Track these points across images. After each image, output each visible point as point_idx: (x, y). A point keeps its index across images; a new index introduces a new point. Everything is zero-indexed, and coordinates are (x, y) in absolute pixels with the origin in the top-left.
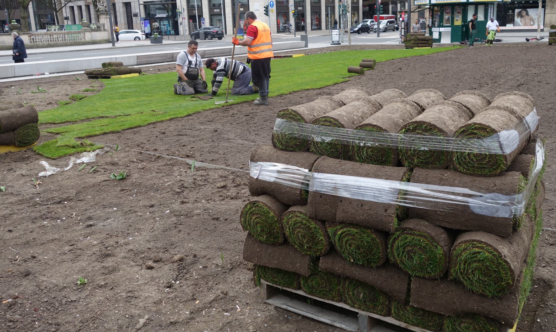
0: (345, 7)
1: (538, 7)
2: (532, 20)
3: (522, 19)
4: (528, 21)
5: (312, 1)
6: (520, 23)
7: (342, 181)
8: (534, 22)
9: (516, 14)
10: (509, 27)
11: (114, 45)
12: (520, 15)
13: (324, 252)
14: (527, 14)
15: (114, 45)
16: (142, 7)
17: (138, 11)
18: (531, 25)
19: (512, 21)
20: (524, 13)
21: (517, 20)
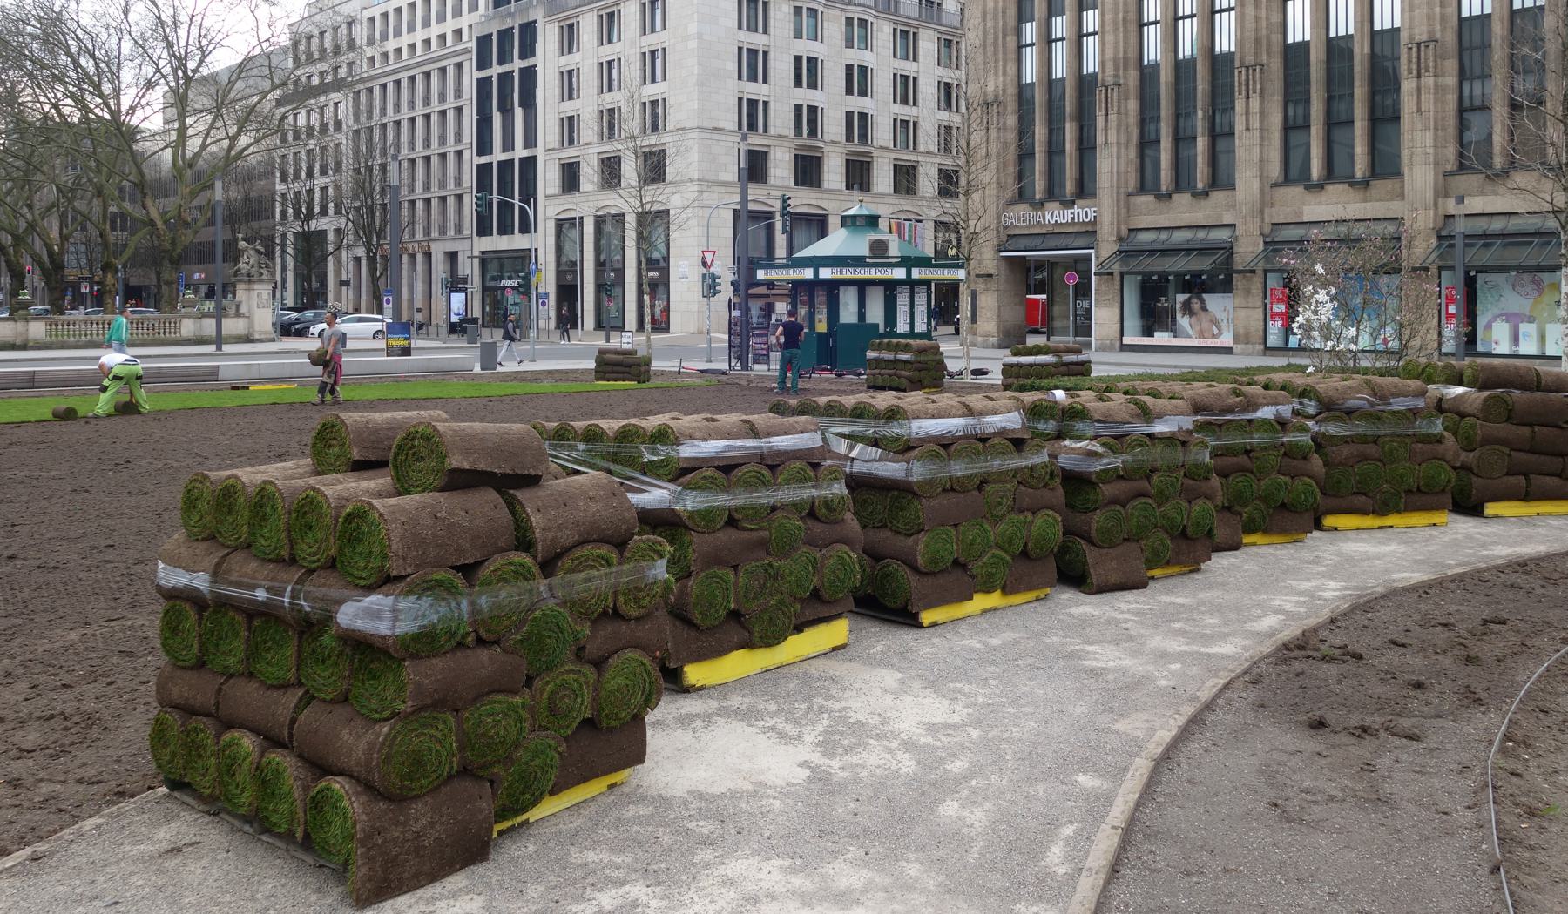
0: (714, 277)
1: (213, 261)
2: (1215, 322)
3: (1194, 319)
4: (1206, 325)
5: (1517, 5)
6: (1189, 331)
7: (711, 286)
8: (1219, 327)
9: (1178, 306)
10: (1161, 338)
11: (219, 348)
12: (1187, 308)
13: (363, 829)
14: (1204, 308)
15: (219, 348)
16: (476, 261)
17: (468, 272)
18: (1213, 336)
19: (1172, 327)
20: (1196, 305)
21: (1183, 321)
